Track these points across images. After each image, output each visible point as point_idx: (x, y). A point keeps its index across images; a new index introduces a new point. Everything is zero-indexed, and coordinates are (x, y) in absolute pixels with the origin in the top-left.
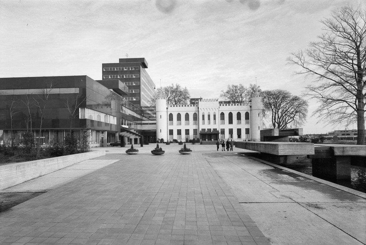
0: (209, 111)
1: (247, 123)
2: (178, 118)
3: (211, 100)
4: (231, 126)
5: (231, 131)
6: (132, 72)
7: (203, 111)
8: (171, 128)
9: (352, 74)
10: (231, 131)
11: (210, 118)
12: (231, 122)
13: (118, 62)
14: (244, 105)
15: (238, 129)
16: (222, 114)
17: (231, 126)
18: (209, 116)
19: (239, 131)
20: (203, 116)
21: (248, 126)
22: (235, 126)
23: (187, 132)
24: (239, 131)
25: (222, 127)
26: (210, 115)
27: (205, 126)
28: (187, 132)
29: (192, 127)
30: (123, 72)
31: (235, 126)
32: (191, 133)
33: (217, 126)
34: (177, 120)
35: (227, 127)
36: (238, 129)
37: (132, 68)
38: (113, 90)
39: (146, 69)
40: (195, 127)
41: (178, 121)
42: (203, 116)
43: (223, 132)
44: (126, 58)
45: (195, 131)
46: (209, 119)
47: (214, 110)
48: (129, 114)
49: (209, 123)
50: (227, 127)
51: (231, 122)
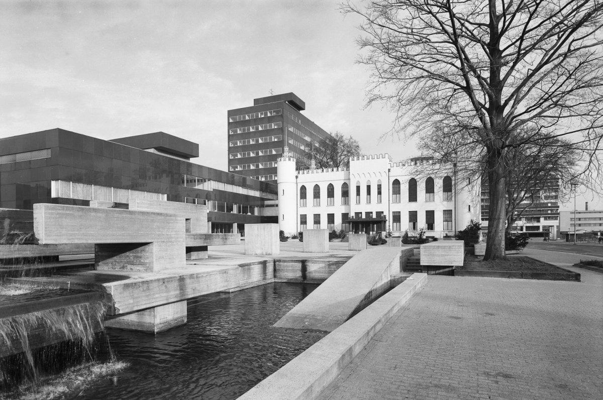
0: (379, 177)
1: (448, 199)
2: (301, 193)
3: (376, 157)
4: (413, 206)
5: (413, 216)
6: (270, 120)
7: (358, 178)
8: (302, 211)
9: (445, 37)
10: (413, 216)
11: (378, 189)
12: (413, 197)
13: (252, 104)
14: (359, 160)
15: (427, 212)
16: (397, 183)
17: (413, 206)
18: (369, 187)
19: (430, 215)
20: (358, 188)
21: (449, 206)
22: (421, 206)
23: (331, 218)
24: (430, 215)
25: (395, 208)
26: (359, 186)
27: (360, 207)
28: (331, 218)
29: (338, 209)
30: (257, 121)
31: (421, 206)
32: (338, 220)
33: (384, 205)
34: (426, 193)
35: (405, 207)
36: (427, 212)
37: (271, 113)
38: (156, 148)
39: (301, 112)
40: (343, 210)
41: (315, 199)
42: (358, 188)
43: (397, 218)
44: (270, 95)
45: (345, 216)
46: (369, 192)
47: (378, 174)
48: (213, 189)
49: (369, 201)
50: (405, 207)
51: (413, 197)
